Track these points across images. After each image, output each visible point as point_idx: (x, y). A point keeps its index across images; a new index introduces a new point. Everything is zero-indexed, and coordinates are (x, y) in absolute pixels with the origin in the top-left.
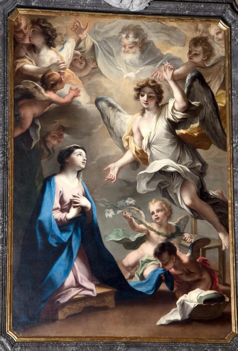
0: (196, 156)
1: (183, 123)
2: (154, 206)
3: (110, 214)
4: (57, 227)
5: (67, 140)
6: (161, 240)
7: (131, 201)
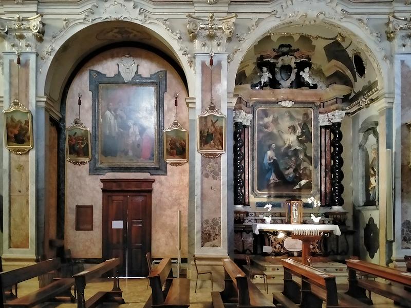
0: (304, 145)
1: (301, 137)
2: (293, 159)
3: (282, 161)
4: (199, 235)
5: (270, 142)
6: (294, 167)
7: (287, 158)
